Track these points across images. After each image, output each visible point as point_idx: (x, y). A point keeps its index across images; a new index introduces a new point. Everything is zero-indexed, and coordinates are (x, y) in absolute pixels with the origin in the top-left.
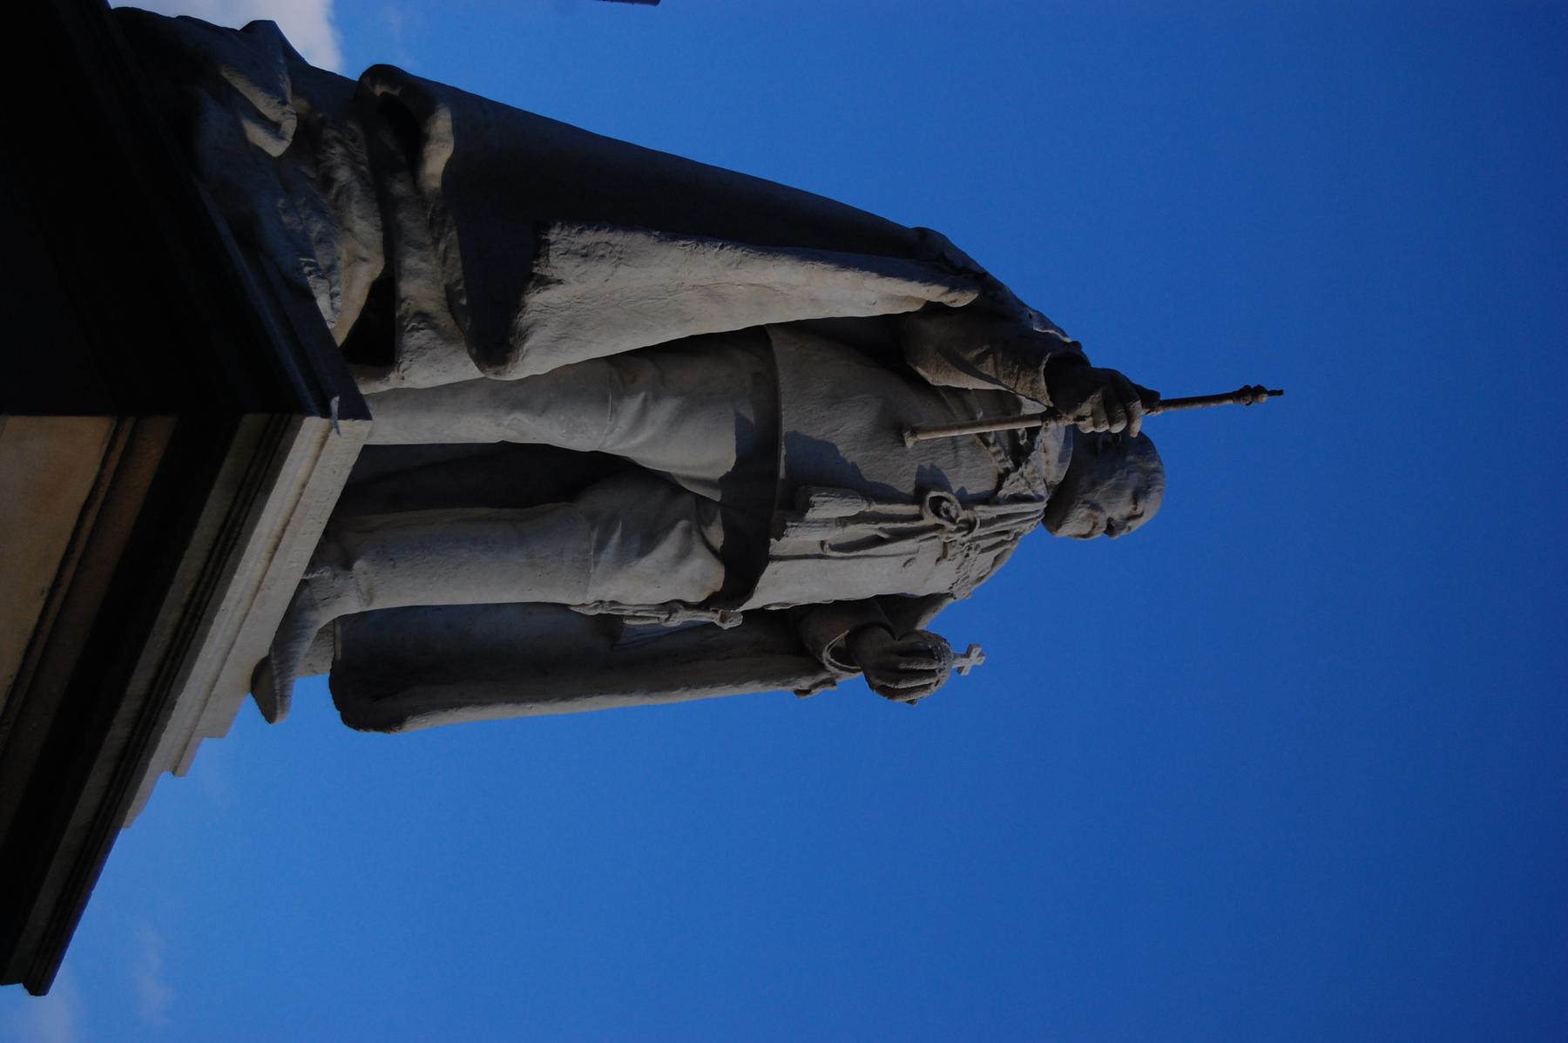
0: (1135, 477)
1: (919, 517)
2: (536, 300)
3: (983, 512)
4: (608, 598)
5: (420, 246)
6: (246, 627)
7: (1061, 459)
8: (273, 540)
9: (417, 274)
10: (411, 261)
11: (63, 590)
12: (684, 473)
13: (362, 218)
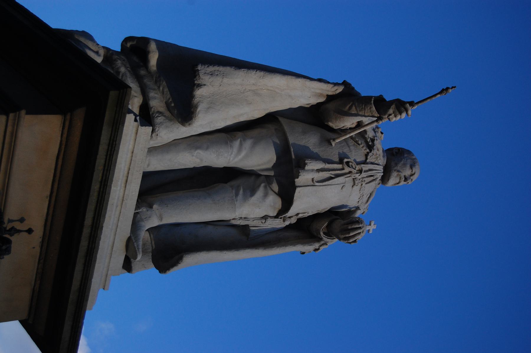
0: (409, 161)
1: (343, 169)
2: (199, 93)
3: (365, 167)
4: (243, 216)
5: (154, 89)
6: (121, 219)
7: (383, 157)
8: (125, 178)
9: (155, 98)
10: (152, 94)
11: (54, 194)
12: (259, 168)
13: (132, 83)
